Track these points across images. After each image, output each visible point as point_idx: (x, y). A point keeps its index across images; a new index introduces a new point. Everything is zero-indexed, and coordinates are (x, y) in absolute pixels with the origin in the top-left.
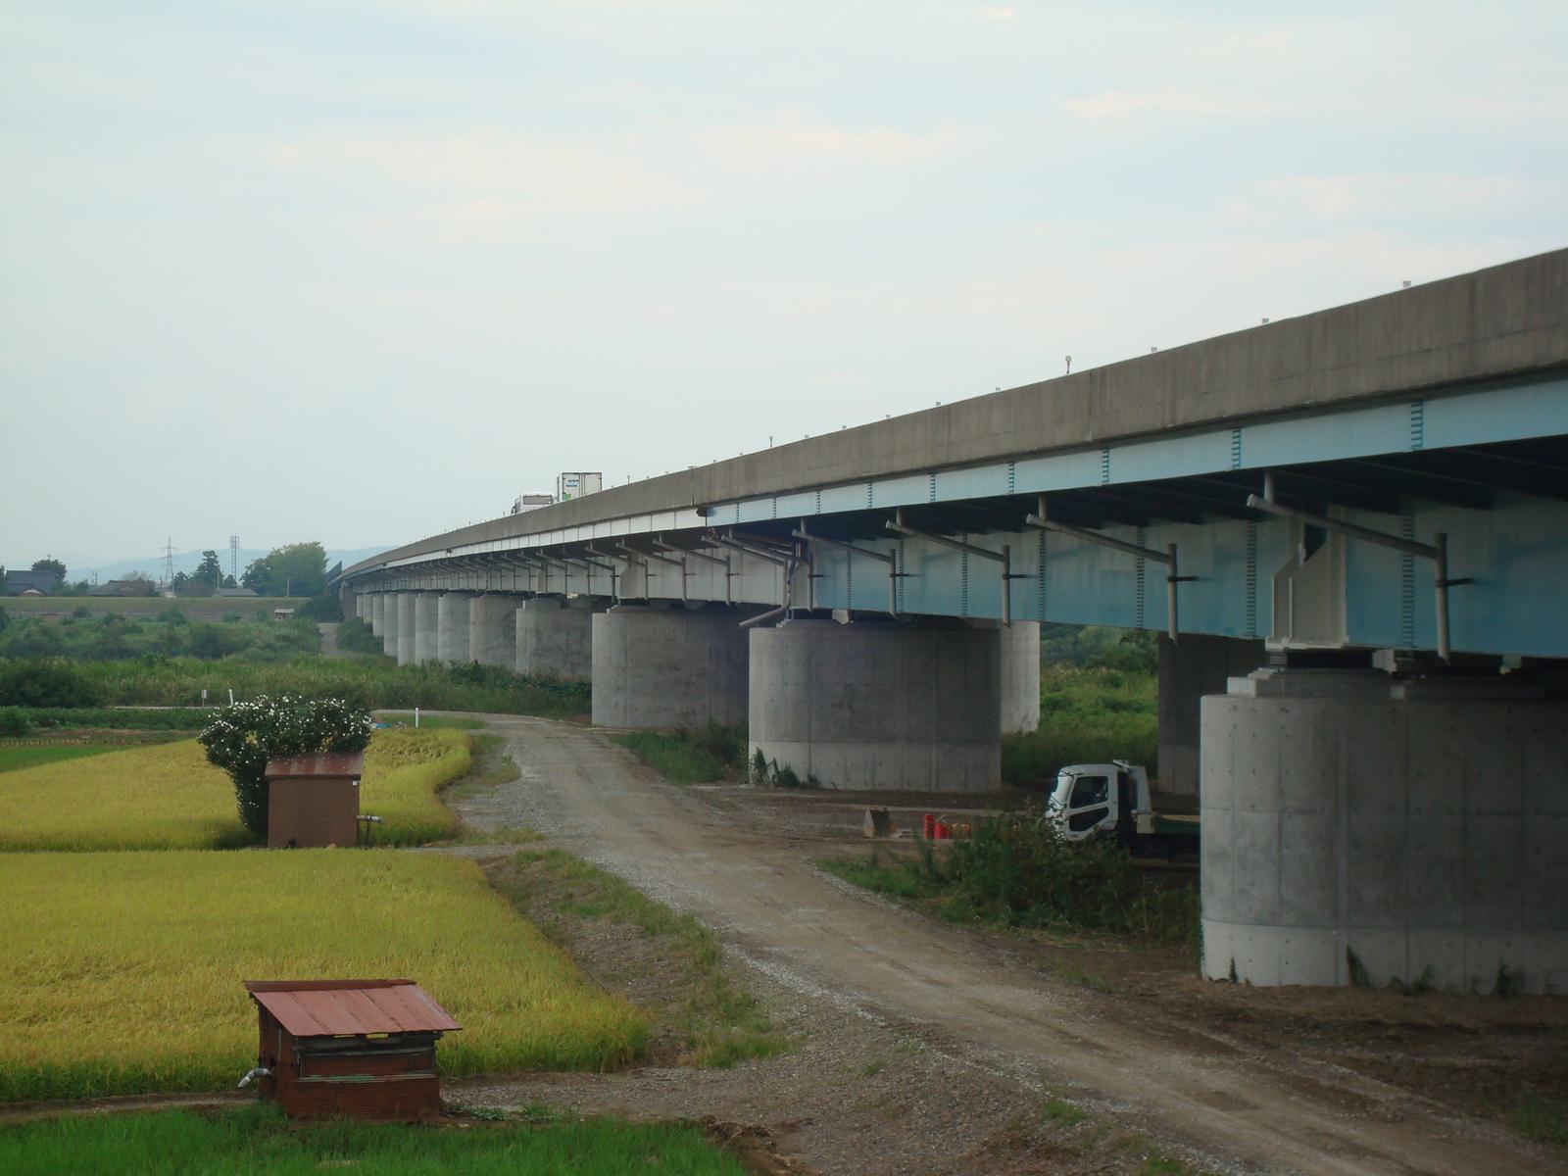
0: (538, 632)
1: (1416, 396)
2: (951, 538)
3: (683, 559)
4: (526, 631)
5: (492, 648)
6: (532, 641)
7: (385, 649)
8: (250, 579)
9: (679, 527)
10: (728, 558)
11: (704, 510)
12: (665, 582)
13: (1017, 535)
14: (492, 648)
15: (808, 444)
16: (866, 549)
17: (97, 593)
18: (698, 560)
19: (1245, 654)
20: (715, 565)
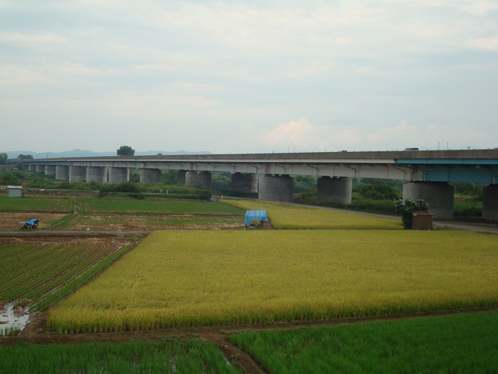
0: (191, 179)
1: (427, 159)
2: (349, 166)
3: (355, 168)
4: (188, 178)
5: (145, 180)
6: (190, 180)
7: (56, 178)
8: (118, 154)
9: (366, 162)
10: (355, 168)
11: (136, 160)
12: (63, 164)
13: (338, 166)
14: (145, 180)
15: (239, 154)
16: (352, 168)
17: (219, 164)
18: (228, 165)
19: (56, 166)
20: (314, 168)
